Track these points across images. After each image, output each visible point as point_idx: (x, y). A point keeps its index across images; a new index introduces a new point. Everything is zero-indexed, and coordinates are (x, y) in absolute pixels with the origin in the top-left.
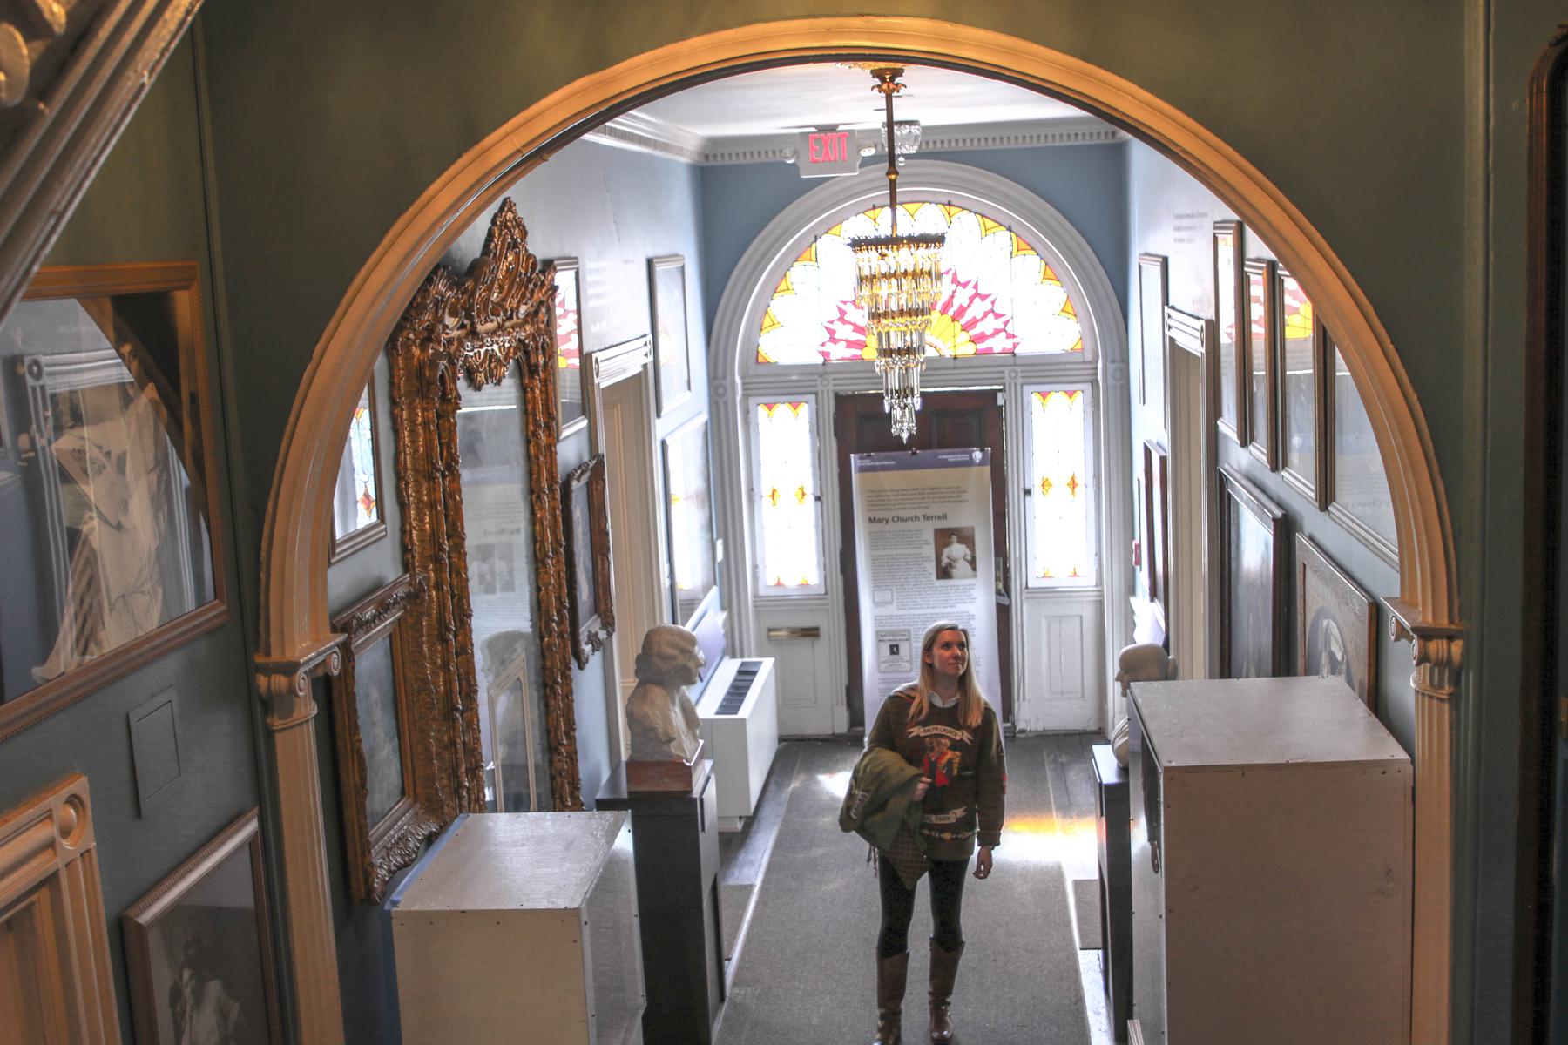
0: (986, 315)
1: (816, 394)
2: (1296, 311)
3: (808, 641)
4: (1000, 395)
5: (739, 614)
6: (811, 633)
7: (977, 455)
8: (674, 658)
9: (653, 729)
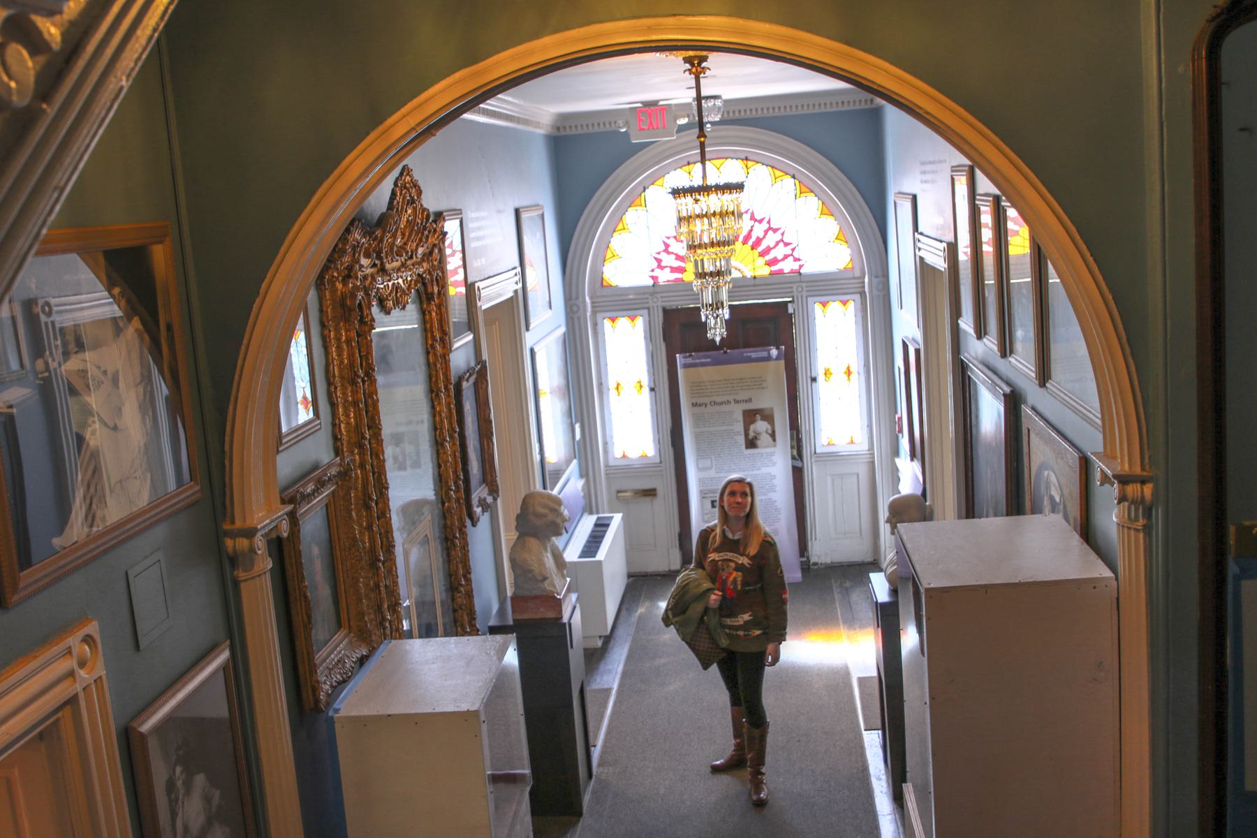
3: (648, 499)
6: (650, 493)
8: (545, 516)
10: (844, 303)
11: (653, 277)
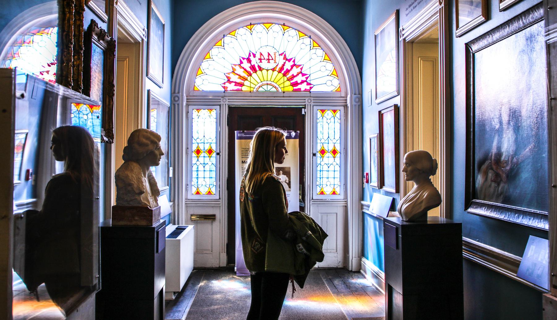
0: (298, 75)
1: (220, 105)
2: (338, 285)
3: (210, 221)
4: (303, 109)
5: (178, 205)
6: (211, 218)
7: (293, 134)
8: (147, 145)
9: (130, 185)
10: (335, 111)
11: (224, 87)
